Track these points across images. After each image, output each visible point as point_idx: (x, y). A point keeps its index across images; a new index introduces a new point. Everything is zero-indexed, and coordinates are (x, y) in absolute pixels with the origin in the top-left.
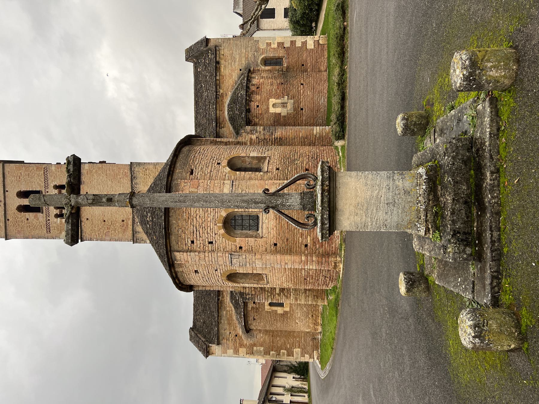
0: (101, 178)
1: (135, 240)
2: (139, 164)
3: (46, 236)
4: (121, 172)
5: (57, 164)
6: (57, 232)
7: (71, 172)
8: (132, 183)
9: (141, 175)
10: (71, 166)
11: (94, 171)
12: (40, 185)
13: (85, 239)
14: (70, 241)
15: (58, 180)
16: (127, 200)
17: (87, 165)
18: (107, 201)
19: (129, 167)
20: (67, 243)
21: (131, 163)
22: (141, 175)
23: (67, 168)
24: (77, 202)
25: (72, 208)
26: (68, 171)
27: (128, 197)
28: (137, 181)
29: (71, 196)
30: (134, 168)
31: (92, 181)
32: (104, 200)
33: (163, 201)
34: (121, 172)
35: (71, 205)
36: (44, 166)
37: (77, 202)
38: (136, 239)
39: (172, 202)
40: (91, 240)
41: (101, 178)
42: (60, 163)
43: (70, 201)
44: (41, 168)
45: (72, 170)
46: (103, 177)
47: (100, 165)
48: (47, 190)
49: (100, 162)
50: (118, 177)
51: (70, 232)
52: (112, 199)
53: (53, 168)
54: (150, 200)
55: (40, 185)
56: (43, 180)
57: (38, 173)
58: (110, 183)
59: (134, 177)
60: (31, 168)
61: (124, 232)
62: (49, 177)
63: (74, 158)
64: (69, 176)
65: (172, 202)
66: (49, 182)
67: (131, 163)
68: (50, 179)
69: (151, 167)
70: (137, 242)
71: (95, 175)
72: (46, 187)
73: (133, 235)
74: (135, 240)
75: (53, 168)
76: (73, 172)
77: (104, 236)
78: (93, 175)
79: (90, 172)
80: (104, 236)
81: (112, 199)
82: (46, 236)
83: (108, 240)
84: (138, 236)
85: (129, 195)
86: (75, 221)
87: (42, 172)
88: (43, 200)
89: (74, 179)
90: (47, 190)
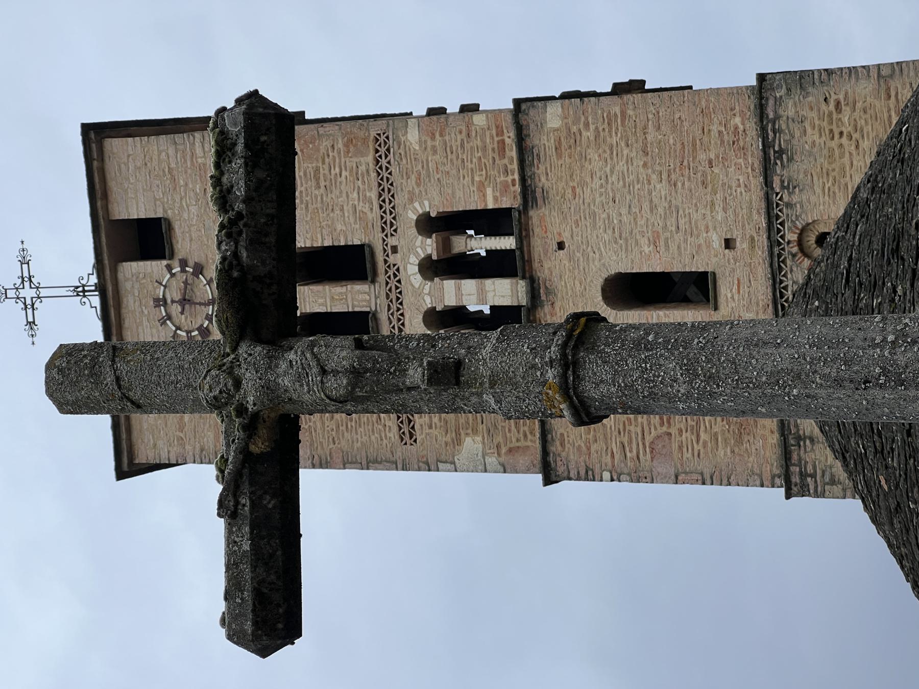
0: (621, 166)
1: (795, 482)
2: (801, 80)
3: (398, 455)
4: (715, 128)
5: (432, 112)
6: (443, 439)
7: (239, 206)
8: (768, 182)
9: (812, 135)
10: (238, 164)
11: (589, 134)
12: (361, 218)
13: (561, 469)
14: (248, 627)
15: (434, 192)
16: (551, 375)
17: (554, 112)
18: (430, 382)
19: (752, 103)
20: (235, 637)
21: (761, 77)
22: (812, 135)
23: (217, 181)
24: (269, 389)
25: (252, 424)
26: (223, 200)
27: (554, 351)
28: (798, 170)
29: (243, 349)
30: (778, 101)
31: (583, 184)
32: (415, 374)
33: (775, 377)
34: (715, 128)
35: (241, 410)
36: (375, 129)
37: (269, 389)
38: (803, 475)
39: (839, 382)
40: (589, 475)
41: (621, 166)
42: (441, 111)
43: (238, 384)
44: (365, 140)
45: (240, 191)
46: (629, 161)
47: (615, 105)
48: (392, 241)
49: (620, 89)
50: (702, 156)
51: (246, 569)
52: (459, 364)
53: (413, 136)
54: (690, 371)
55: (361, 218)
56: (373, 195)
57: (351, 162)
58: (662, 188)
59: (780, 153)
60: (326, 143)
61: (739, 441)
62: (396, 178)
63: (248, 115)
64: (229, 231)
65: (839, 382)
66: (397, 201)
67: (761, 77)
68: (404, 186)
69: (864, 88)
70: (804, 492)
71: (593, 154)
72: (389, 226)
73: (786, 455)
74: (795, 479)
75: (413, 136)
76: (247, 200)
77: (646, 459)
78: (584, 157)
79: (569, 140)
80: (646, 459)
81: (459, 364)
82: (398, 455)
83: (664, 480)
84: (809, 457)
85: (559, 339)
86: (270, 503)
87: (370, 158)
88: (110, 379)
89: (253, 244)
90: (392, 241)
